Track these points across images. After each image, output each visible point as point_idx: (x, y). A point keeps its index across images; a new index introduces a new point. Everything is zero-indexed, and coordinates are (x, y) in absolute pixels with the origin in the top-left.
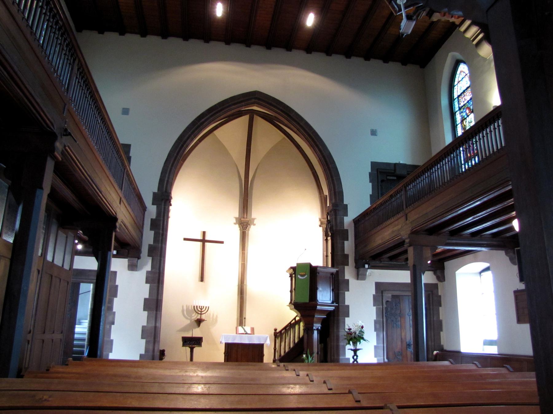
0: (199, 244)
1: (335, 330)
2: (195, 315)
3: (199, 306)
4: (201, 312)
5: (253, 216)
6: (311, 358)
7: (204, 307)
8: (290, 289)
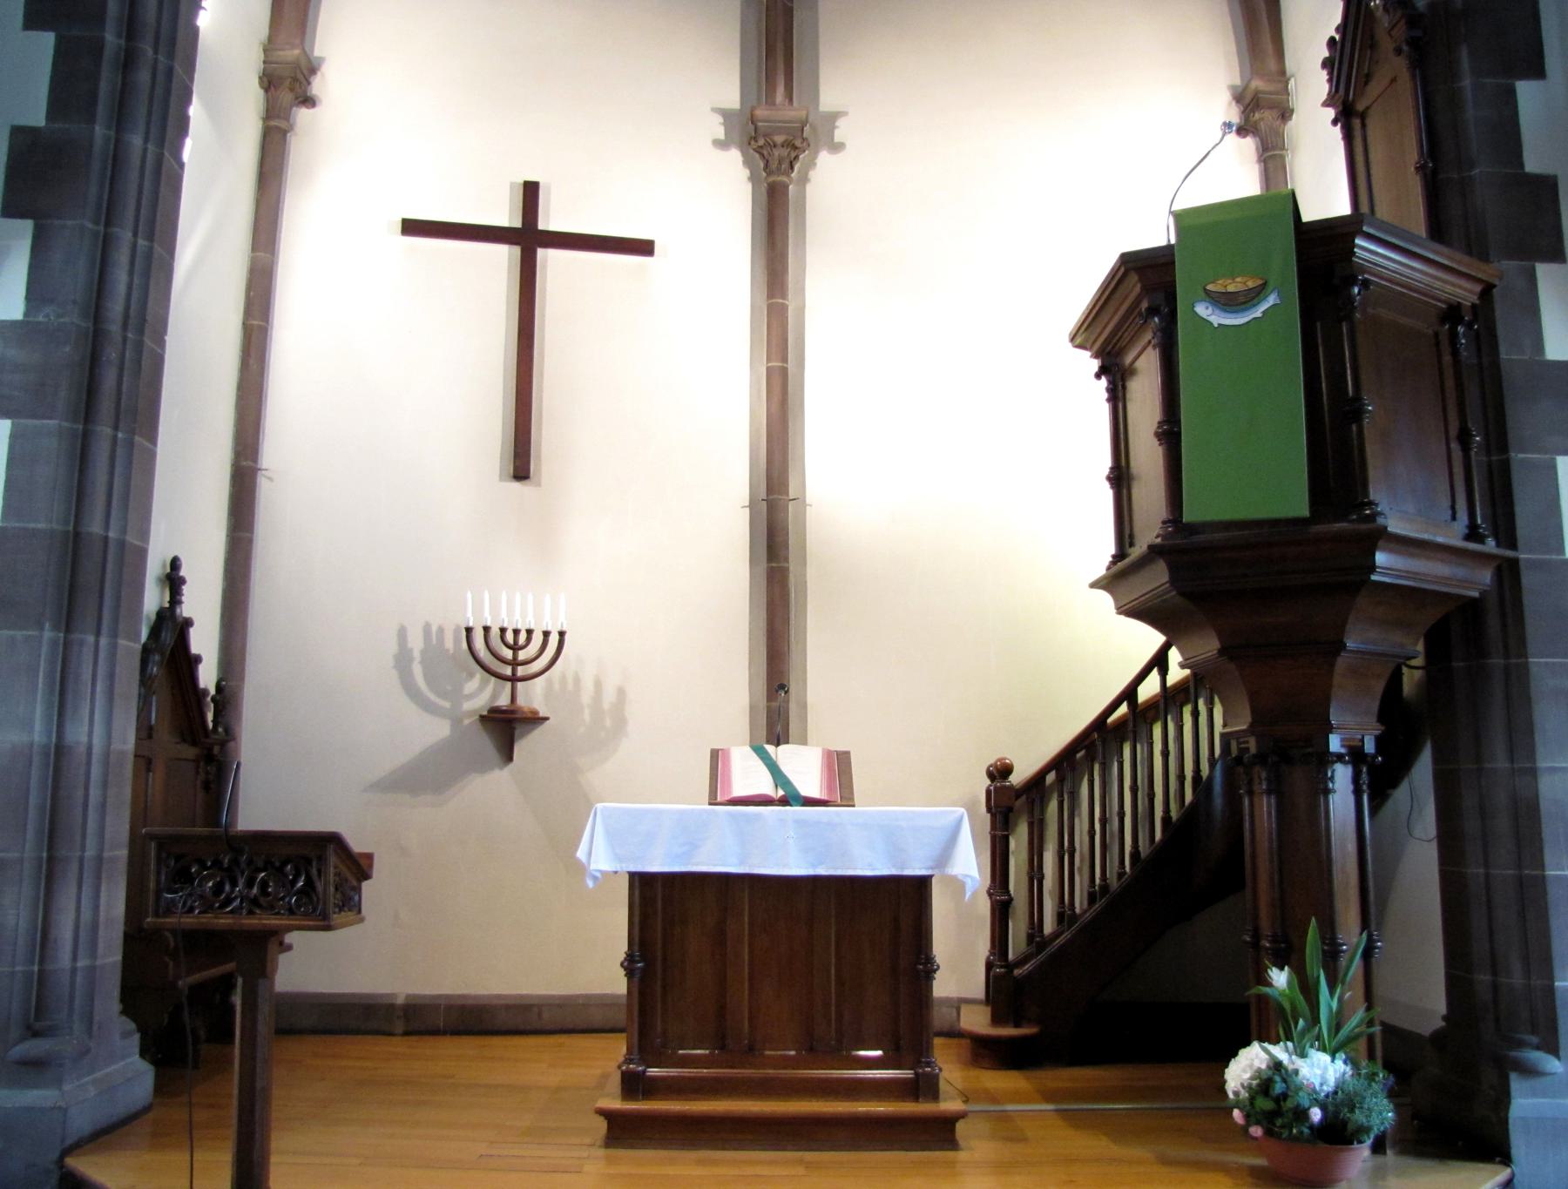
0: (503, 256)
1: (1500, 762)
2: (481, 689)
3: (503, 630)
4: (515, 663)
5: (830, 96)
6: (1332, 993)
7: (530, 632)
8: (1105, 462)
